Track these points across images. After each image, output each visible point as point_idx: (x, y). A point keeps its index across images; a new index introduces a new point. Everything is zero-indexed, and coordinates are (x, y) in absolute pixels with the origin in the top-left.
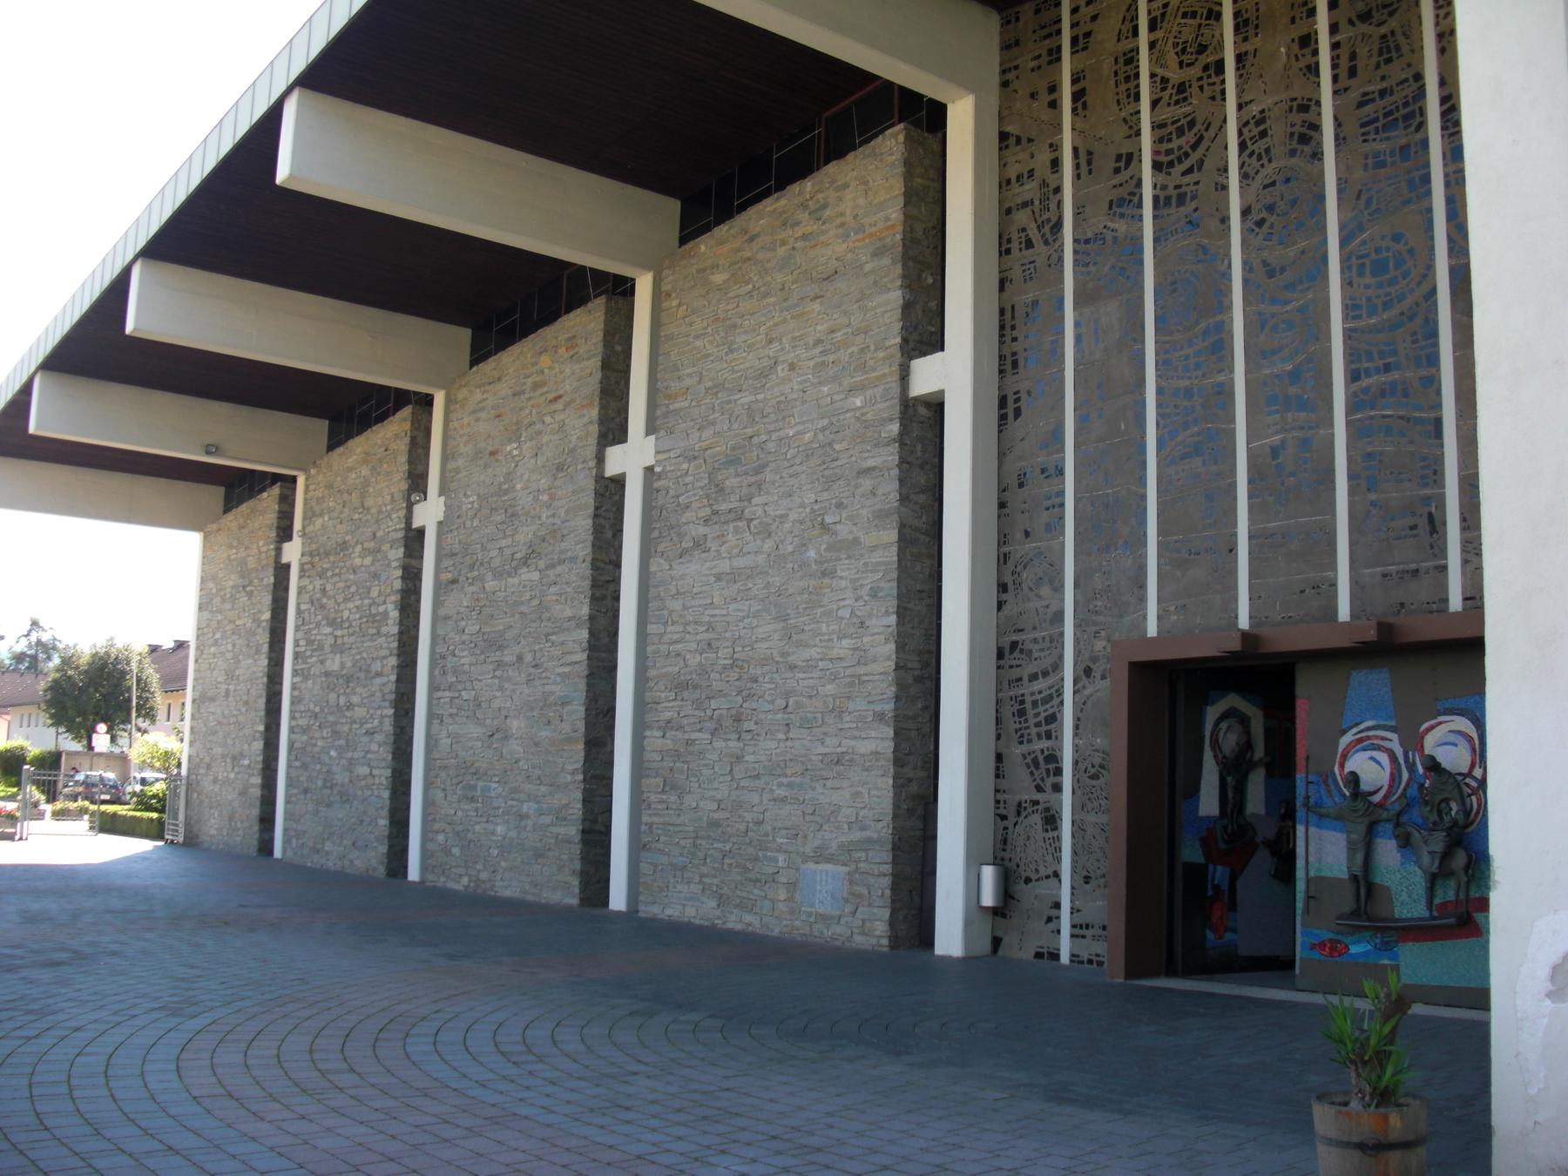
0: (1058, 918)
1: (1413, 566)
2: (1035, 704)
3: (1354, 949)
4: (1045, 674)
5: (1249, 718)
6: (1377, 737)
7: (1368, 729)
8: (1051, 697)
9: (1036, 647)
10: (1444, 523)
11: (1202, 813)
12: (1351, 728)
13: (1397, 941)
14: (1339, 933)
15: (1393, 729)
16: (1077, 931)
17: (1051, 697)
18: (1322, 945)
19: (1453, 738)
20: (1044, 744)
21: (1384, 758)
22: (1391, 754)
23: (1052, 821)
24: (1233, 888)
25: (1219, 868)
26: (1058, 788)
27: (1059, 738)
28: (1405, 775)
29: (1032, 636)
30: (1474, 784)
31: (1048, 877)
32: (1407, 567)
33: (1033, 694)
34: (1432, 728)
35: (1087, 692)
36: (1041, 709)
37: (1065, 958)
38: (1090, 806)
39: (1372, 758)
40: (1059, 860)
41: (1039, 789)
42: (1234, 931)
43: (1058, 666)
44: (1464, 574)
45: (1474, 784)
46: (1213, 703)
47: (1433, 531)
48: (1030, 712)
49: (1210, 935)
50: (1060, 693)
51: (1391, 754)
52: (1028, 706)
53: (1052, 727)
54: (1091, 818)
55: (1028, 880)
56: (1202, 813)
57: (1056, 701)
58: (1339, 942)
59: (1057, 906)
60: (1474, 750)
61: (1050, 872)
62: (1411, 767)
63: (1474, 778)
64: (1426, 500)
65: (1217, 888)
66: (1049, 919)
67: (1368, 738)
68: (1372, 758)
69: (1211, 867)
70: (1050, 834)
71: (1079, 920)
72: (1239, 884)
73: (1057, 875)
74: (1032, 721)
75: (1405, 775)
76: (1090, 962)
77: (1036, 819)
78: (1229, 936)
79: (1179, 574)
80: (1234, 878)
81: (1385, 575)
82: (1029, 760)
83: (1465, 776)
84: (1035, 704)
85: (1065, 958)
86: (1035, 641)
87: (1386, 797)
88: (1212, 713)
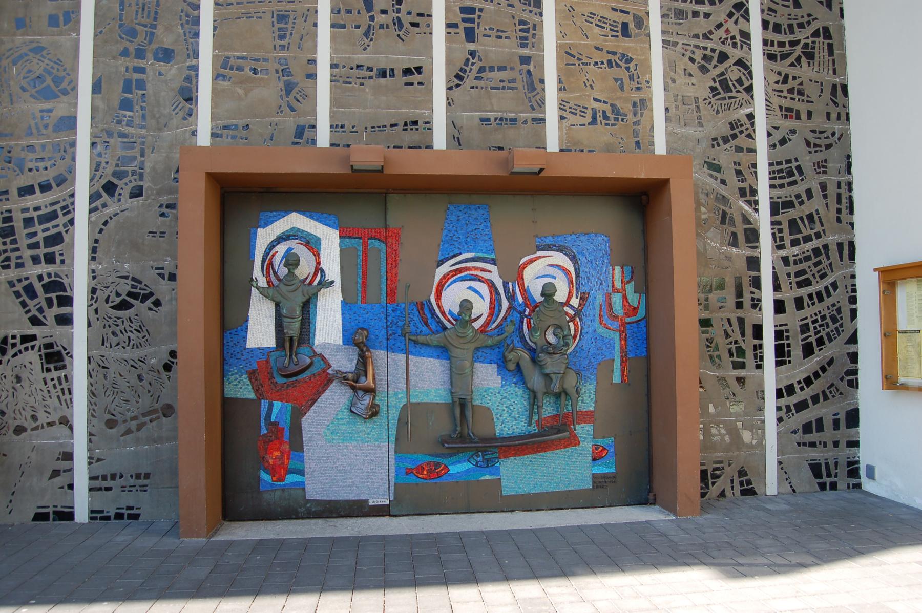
0: (71, 470)
1: (512, 115)
2: (28, 222)
3: (454, 469)
4: (45, 188)
5: (318, 240)
6: (476, 269)
7: (466, 261)
8: (53, 216)
9: (31, 156)
10: (542, 81)
11: (251, 343)
12: (447, 259)
13: (499, 458)
14: (437, 456)
15: (493, 262)
16: (97, 484)
17: (53, 216)
18: (420, 469)
19: (552, 271)
20: (44, 269)
21: (484, 289)
22: (491, 285)
23: (55, 357)
24: (296, 429)
25: (277, 405)
26: (66, 320)
27: (67, 261)
28: (505, 304)
29: (25, 142)
30: (572, 312)
31: (50, 424)
32: (505, 115)
33: (25, 210)
34: (531, 261)
35: (110, 210)
36: (38, 228)
37: (82, 515)
38: (114, 340)
39: (470, 288)
40: (70, 404)
41: (35, 321)
42: (301, 473)
43: (65, 179)
44: (560, 128)
45: (572, 312)
46: (266, 225)
47: (531, 87)
48: (21, 232)
49: (265, 476)
50: (68, 210)
51: (491, 285)
52: (18, 224)
53: (56, 249)
54: (113, 354)
55: (19, 430)
56: (251, 343)
57: (62, 220)
58: (438, 465)
59: (68, 456)
60: (571, 282)
61: (55, 418)
62: (511, 298)
63: (572, 307)
64: (525, 60)
65: (274, 427)
66: (56, 473)
67: (466, 269)
68: (470, 288)
69: (264, 404)
70: (55, 374)
71: (100, 470)
72: (306, 421)
73: (66, 422)
74: (23, 242)
75: (505, 304)
76: (119, 516)
77: (33, 357)
78: (291, 478)
79: (241, 92)
80: (298, 415)
81: (482, 120)
82: (19, 287)
83: (563, 304)
84: (28, 222)
85: (82, 515)
86: (31, 148)
87: (487, 323)
88: (264, 236)
